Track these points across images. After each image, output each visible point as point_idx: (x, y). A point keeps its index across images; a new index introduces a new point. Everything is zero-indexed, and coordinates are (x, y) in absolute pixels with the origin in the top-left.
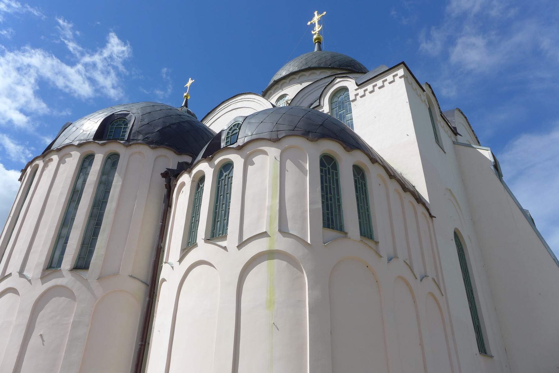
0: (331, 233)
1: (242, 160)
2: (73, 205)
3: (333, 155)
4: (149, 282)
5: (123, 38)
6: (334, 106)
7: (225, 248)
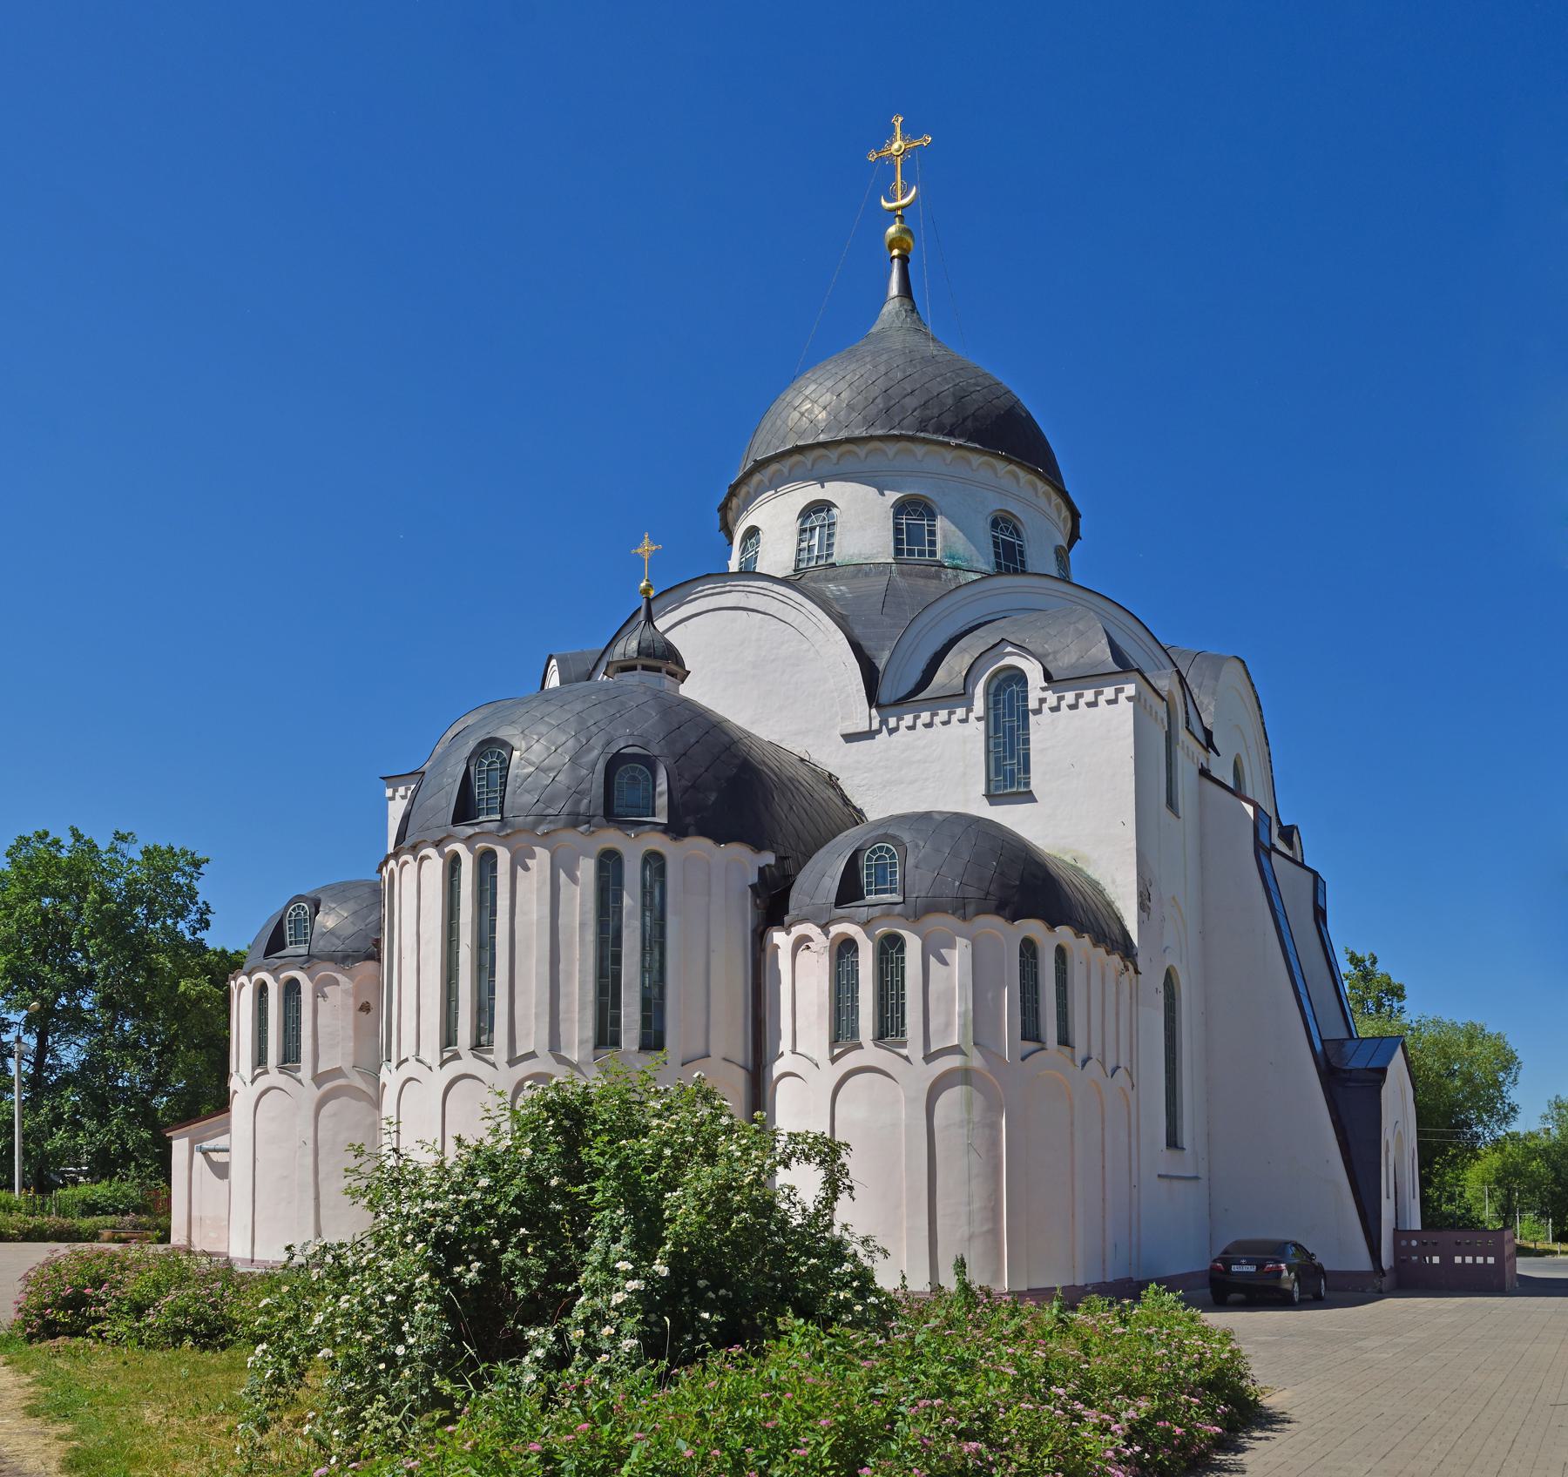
0: (1176, 1153)
1: (508, 855)
2: (486, 975)
3: (1039, 944)
4: (750, 1065)
5: (653, 540)
6: (217, 1088)
7: (906, 1058)
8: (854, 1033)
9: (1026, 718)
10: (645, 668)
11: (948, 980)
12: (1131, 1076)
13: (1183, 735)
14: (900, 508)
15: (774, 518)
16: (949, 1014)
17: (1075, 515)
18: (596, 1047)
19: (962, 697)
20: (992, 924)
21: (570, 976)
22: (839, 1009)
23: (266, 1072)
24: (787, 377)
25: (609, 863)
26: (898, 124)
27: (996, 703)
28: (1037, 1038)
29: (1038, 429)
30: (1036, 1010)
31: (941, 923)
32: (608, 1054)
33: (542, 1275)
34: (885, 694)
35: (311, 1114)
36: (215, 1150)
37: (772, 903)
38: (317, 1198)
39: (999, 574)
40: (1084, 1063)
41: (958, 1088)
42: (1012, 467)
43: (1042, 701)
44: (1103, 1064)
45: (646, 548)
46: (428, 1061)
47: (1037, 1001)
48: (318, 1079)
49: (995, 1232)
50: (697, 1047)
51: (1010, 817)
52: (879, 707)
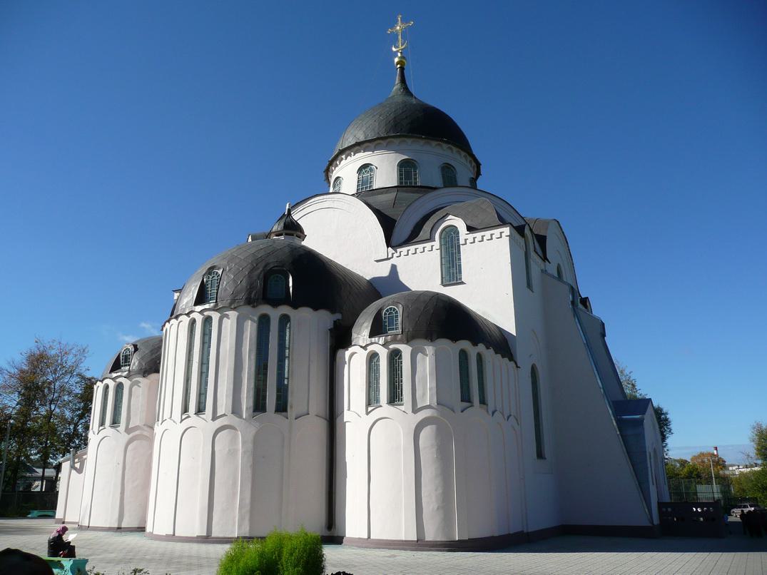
4: (328, 419)
8: (378, 401)
9: (459, 246)
10: (286, 234)
11: (424, 366)
12: (517, 420)
13: (533, 254)
14: (402, 165)
15: (347, 171)
16: (425, 389)
17: (478, 165)
18: (254, 411)
19: (431, 239)
20: (444, 343)
21: (246, 338)
22: (370, 383)
23: (189, 417)
24: (344, 129)
25: (264, 323)
26: (399, 19)
29: (575, 552)
30: (466, 389)
31: (419, 342)
33: (30, 420)
34: (394, 241)
35: (123, 449)
37: (341, 339)
38: (69, 479)
39: (445, 187)
40: (493, 413)
41: (429, 427)
42: (449, 145)
43: (466, 240)
48: (128, 430)
49: (235, 483)
50: (305, 411)
51: (453, 292)
52: (392, 247)
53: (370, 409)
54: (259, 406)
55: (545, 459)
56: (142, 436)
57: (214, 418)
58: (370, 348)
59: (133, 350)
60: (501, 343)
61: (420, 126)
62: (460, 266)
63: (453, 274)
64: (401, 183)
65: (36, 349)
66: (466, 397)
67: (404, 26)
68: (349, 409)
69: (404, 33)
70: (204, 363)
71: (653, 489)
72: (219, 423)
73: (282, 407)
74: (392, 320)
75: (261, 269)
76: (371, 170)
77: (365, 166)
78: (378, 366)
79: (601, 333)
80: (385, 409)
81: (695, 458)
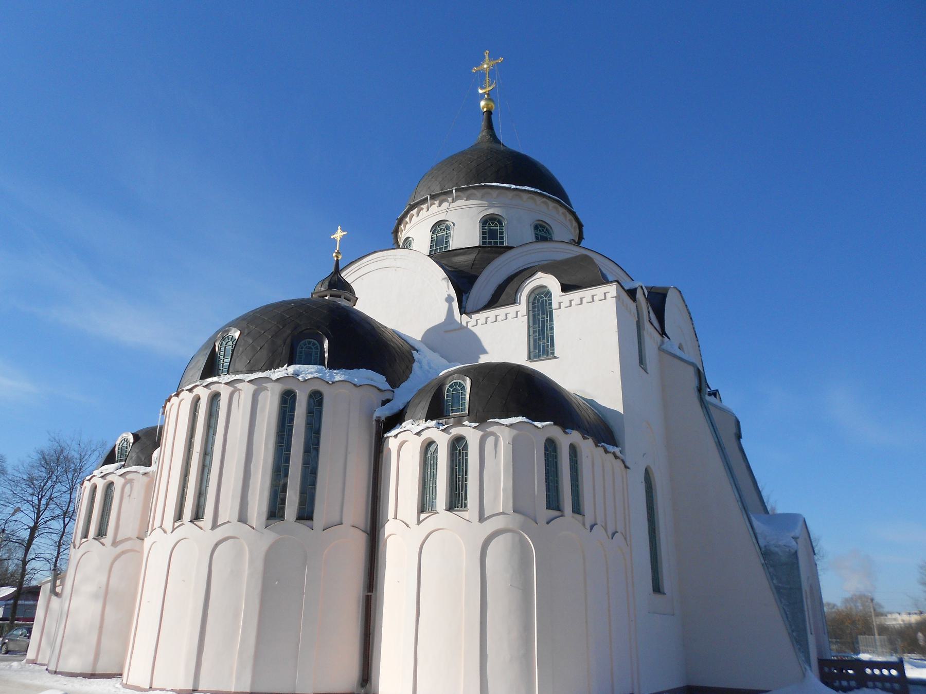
4: (369, 529)
5: (343, 230)
11: (498, 449)
12: (625, 539)
13: (647, 325)
15: (418, 229)
17: (580, 226)
19: (513, 301)
27: (534, 307)
28: (558, 508)
30: (555, 490)
32: (277, 524)
34: (469, 306)
36: (131, 488)
40: (613, 534)
43: (560, 303)
44: (606, 530)
45: (339, 235)
46: (166, 529)
47: (557, 482)
50: (336, 519)
51: (542, 367)
53: (423, 516)
54: (275, 512)
55: (664, 594)
56: (130, 552)
57: (215, 526)
58: (425, 435)
59: (132, 441)
60: (601, 429)
61: (502, 167)
62: (552, 337)
63: (544, 347)
64: (484, 243)
65: (77, 456)
66: (553, 503)
67: (492, 63)
68: (396, 518)
69: (492, 73)
70: (207, 453)
71: (811, 640)
72: (220, 533)
73: (306, 514)
74: (457, 397)
75: (289, 331)
76: (448, 228)
77: (439, 223)
78: (435, 459)
79: (736, 434)
80: (442, 516)
81: (846, 601)
